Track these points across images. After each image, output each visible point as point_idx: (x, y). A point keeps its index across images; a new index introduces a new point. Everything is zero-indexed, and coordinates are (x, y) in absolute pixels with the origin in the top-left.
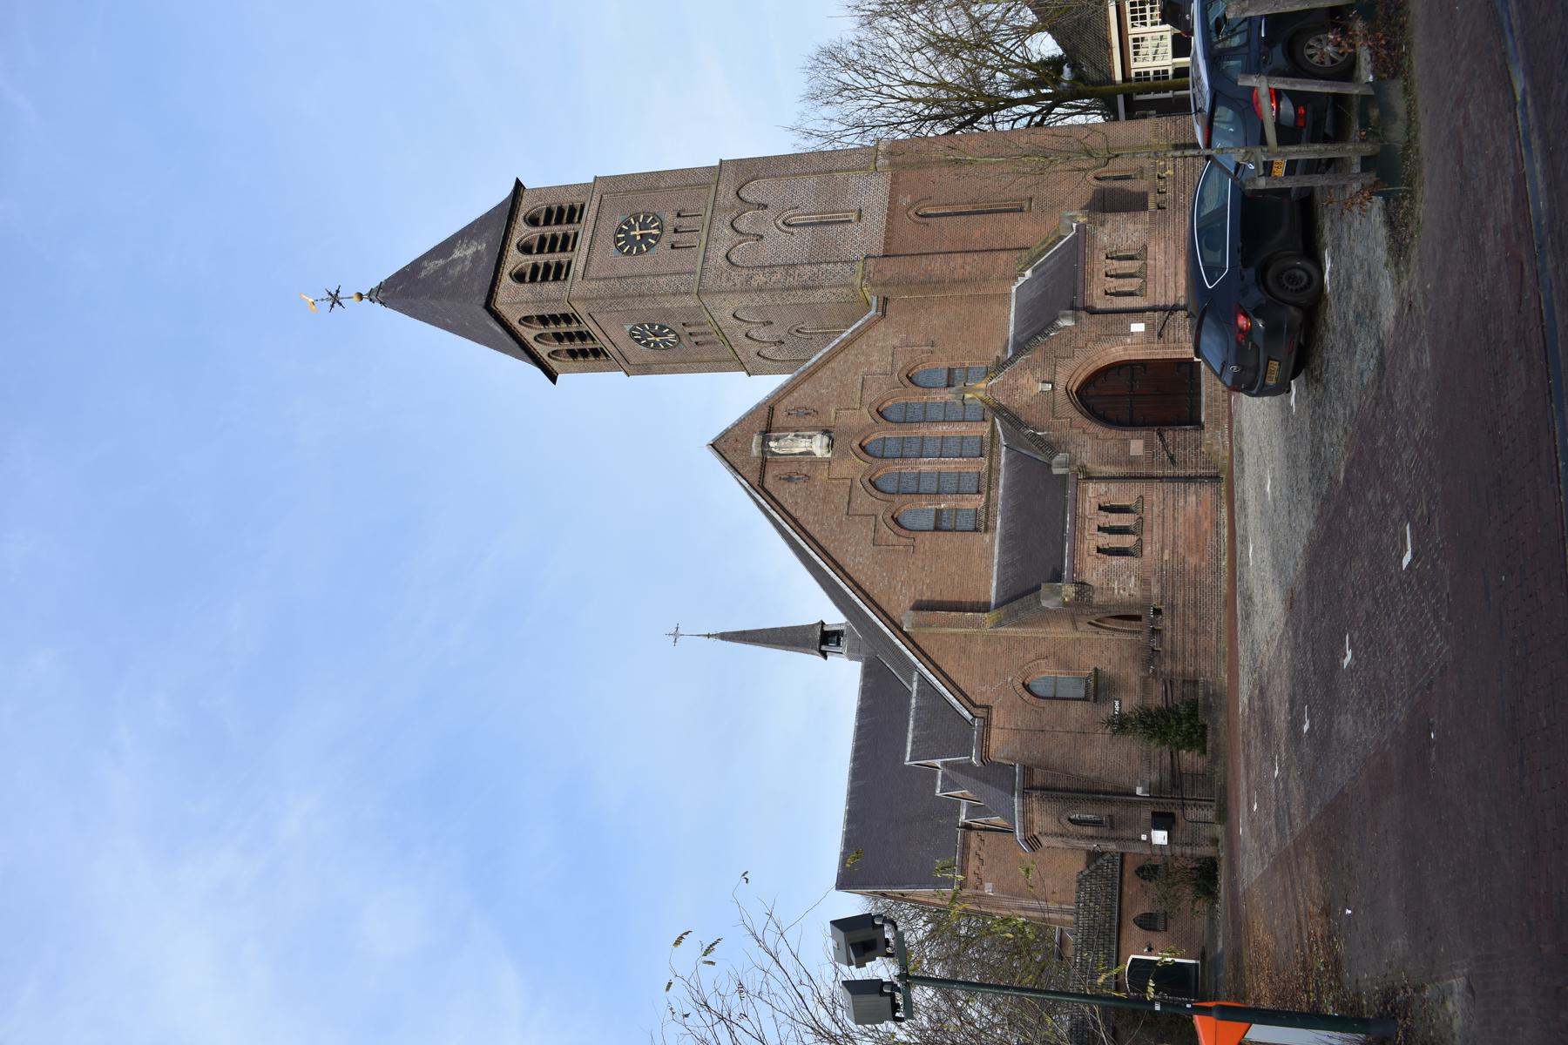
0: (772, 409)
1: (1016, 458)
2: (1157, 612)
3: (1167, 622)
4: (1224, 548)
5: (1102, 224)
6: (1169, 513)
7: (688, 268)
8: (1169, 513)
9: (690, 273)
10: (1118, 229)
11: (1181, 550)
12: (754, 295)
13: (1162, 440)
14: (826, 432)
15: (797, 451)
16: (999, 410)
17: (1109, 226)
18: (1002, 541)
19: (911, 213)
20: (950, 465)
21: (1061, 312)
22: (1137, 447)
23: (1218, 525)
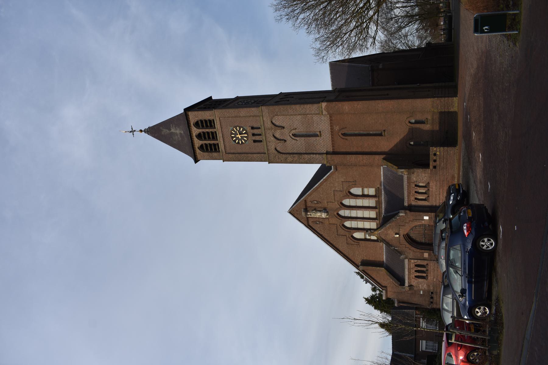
5: (413, 173)
10: (418, 176)
17: (415, 174)
21: (400, 211)
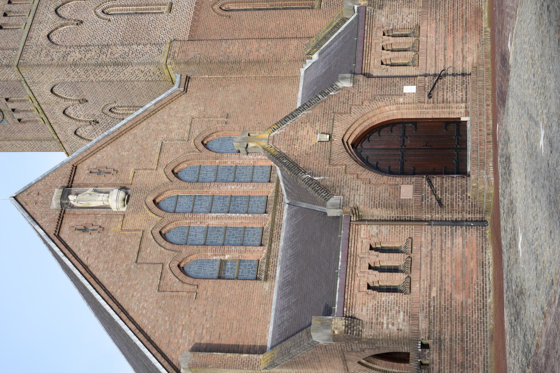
0: (75, 168)
1: (297, 213)
2: (425, 346)
3: (434, 356)
4: (490, 286)
6: (436, 253)
7: (12, 45)
8: (436, 253)
9: (13, 50)
11: (448, 288)
12: (69, 70)
13: (431, 185)
14: (123, 188)
15: (94, 204)
16: (279, 158)
17: (386, 9)
18: (280, 289)
19: (216, 7)
20: (237, 220)
21: (341, 76)
22: (407, 190)
23: (483, 265)
